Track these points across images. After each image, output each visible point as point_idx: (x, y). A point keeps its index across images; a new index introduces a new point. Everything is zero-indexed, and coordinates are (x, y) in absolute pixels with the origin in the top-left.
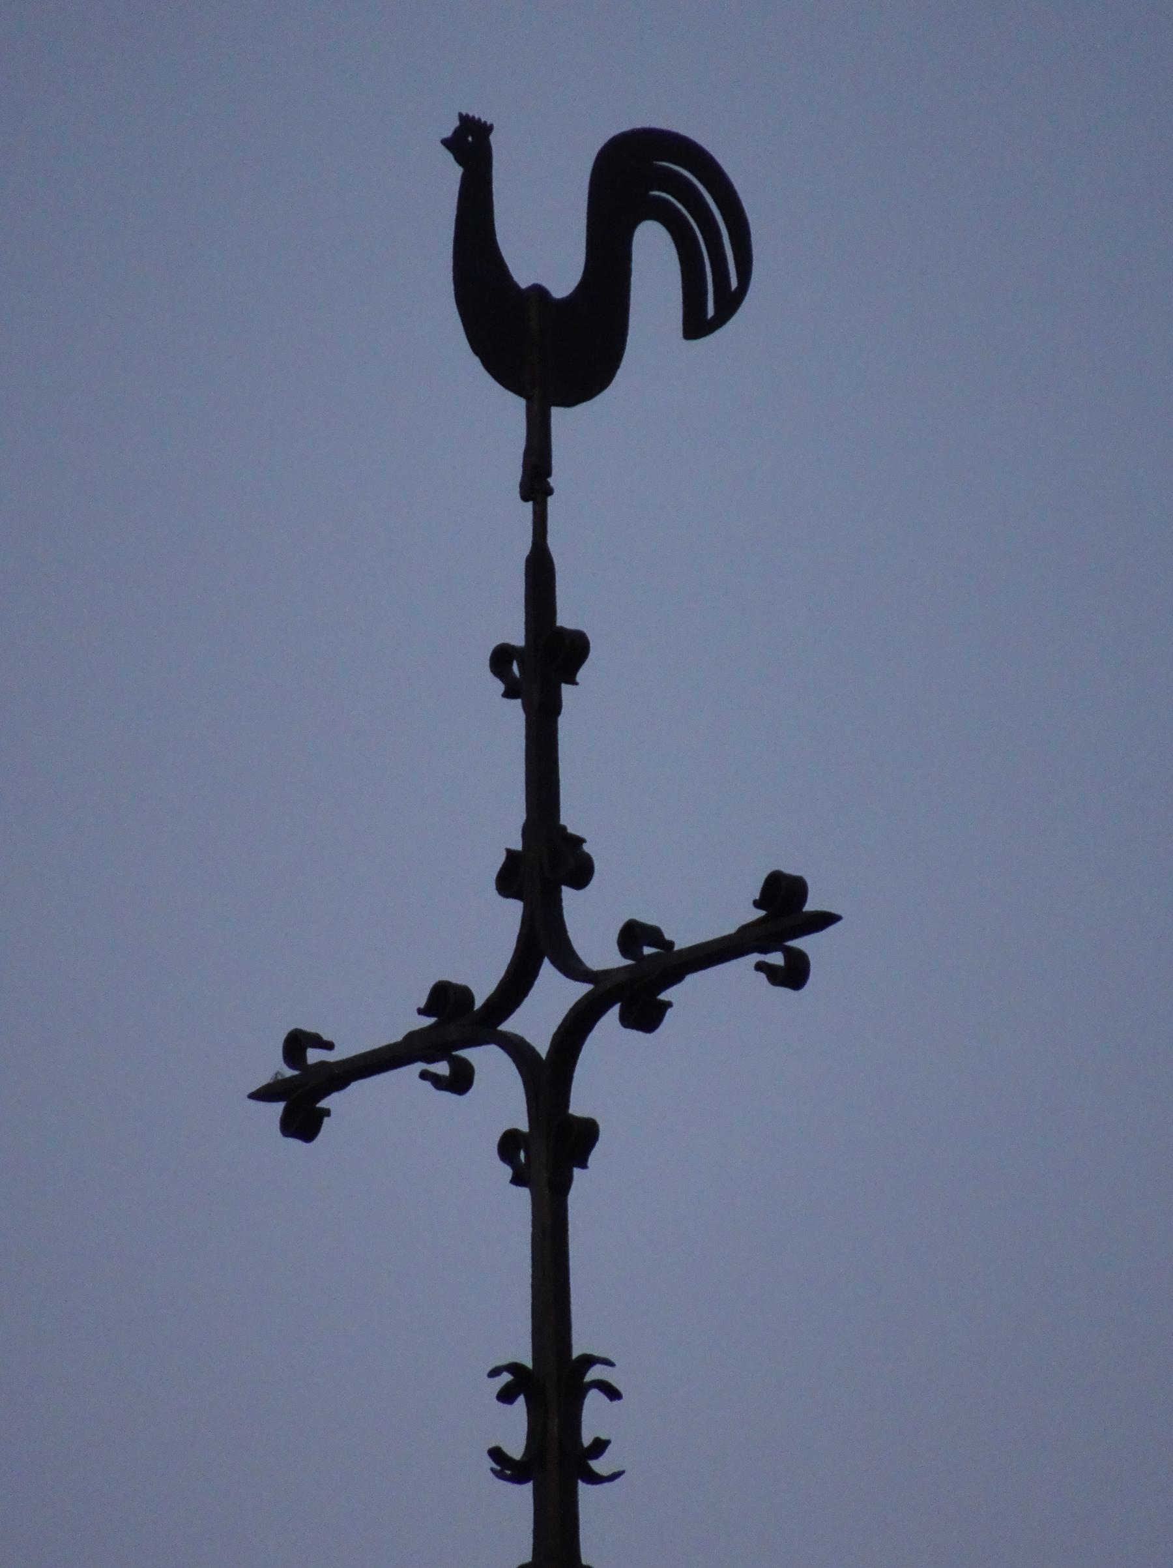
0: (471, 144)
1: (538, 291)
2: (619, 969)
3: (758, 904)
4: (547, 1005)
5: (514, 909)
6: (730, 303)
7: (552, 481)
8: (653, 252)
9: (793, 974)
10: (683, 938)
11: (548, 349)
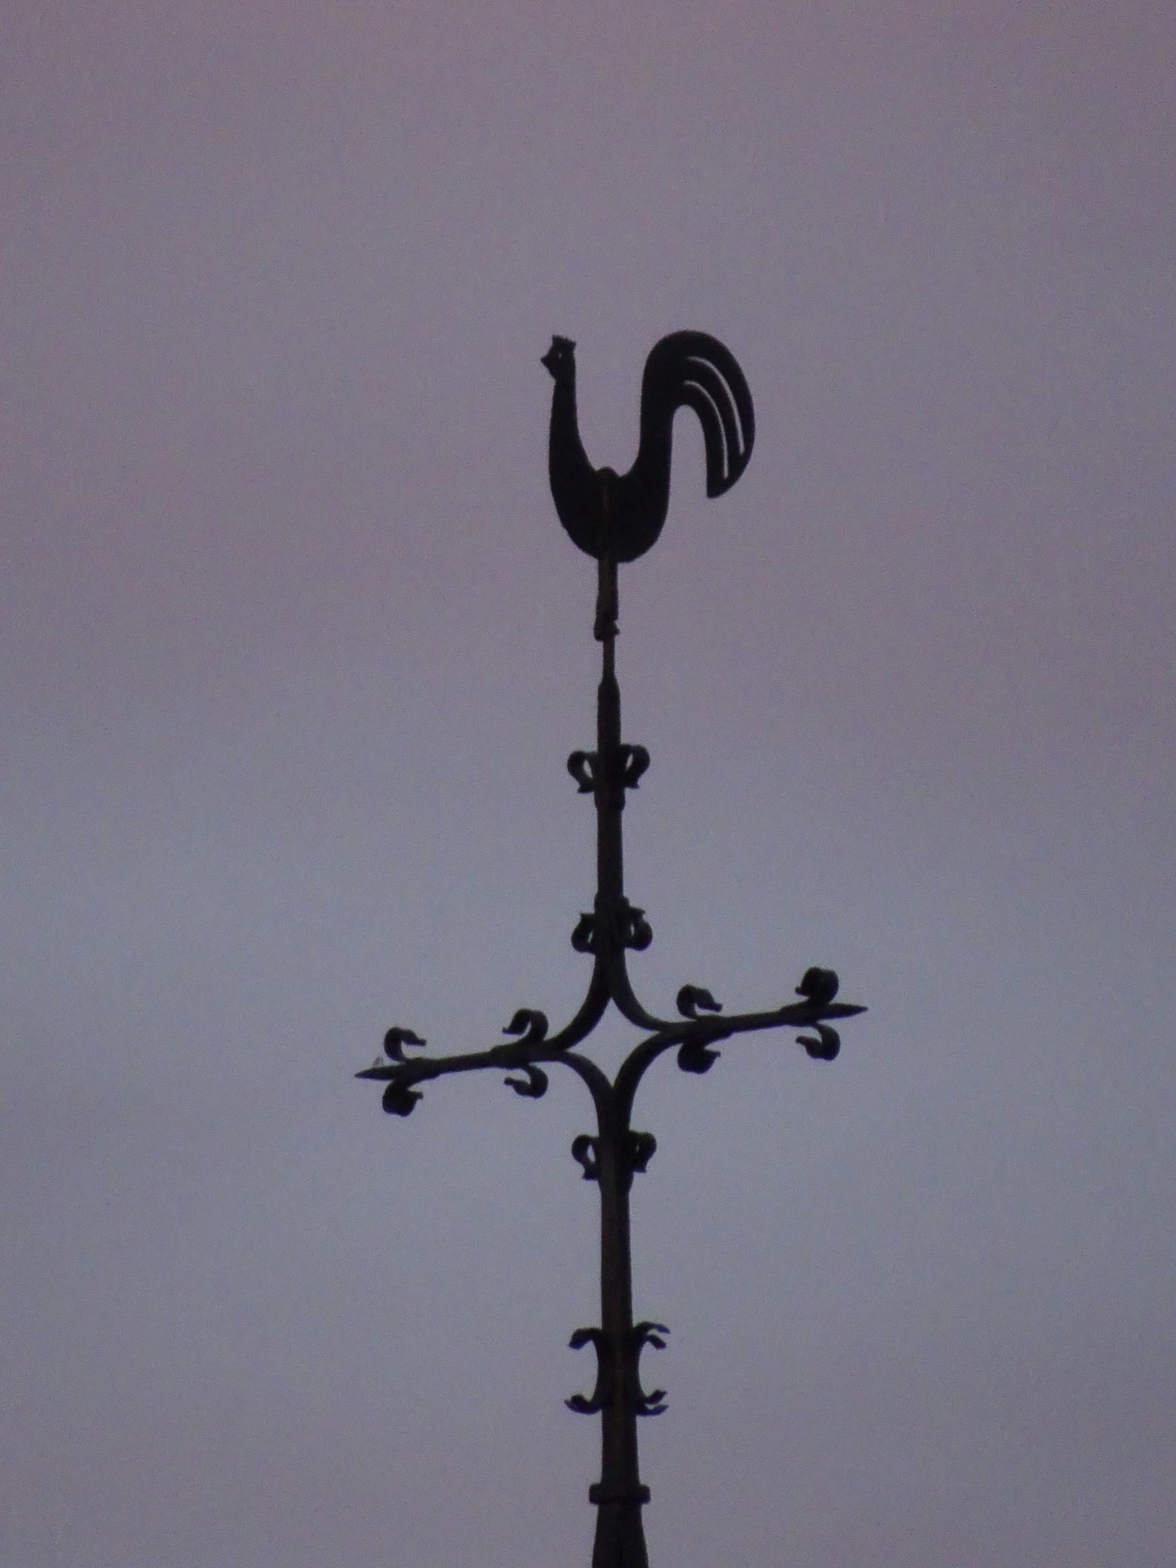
0: (560, 359)
1: (608, 472)
2: (677, 1024)
3: (799, 991)
4: (613, 1042)
5: (588, 961)
6: (739, 463)
7: (619, 624)
8: (686, 426)
9: (826, 1048)
10: (730, 1009)
11: (611, 515)
